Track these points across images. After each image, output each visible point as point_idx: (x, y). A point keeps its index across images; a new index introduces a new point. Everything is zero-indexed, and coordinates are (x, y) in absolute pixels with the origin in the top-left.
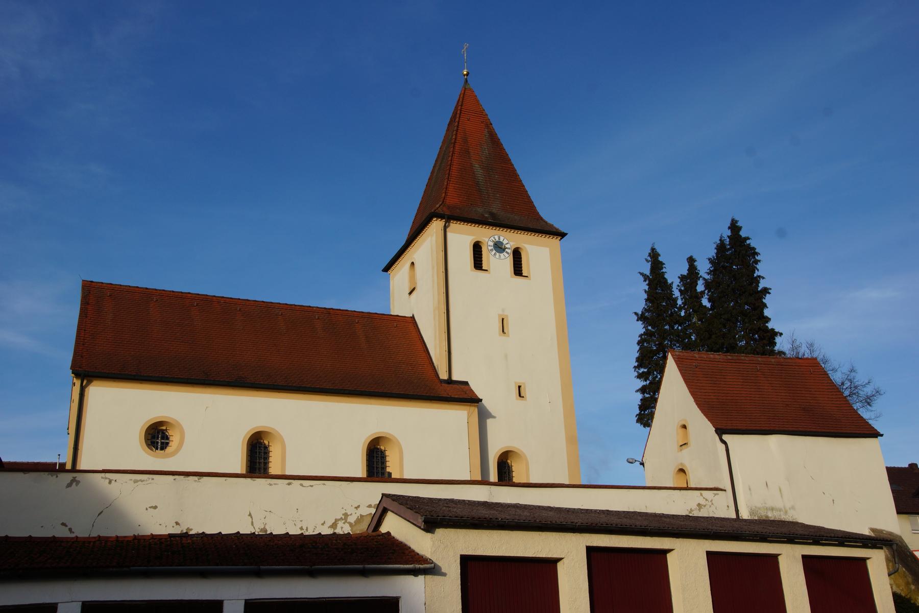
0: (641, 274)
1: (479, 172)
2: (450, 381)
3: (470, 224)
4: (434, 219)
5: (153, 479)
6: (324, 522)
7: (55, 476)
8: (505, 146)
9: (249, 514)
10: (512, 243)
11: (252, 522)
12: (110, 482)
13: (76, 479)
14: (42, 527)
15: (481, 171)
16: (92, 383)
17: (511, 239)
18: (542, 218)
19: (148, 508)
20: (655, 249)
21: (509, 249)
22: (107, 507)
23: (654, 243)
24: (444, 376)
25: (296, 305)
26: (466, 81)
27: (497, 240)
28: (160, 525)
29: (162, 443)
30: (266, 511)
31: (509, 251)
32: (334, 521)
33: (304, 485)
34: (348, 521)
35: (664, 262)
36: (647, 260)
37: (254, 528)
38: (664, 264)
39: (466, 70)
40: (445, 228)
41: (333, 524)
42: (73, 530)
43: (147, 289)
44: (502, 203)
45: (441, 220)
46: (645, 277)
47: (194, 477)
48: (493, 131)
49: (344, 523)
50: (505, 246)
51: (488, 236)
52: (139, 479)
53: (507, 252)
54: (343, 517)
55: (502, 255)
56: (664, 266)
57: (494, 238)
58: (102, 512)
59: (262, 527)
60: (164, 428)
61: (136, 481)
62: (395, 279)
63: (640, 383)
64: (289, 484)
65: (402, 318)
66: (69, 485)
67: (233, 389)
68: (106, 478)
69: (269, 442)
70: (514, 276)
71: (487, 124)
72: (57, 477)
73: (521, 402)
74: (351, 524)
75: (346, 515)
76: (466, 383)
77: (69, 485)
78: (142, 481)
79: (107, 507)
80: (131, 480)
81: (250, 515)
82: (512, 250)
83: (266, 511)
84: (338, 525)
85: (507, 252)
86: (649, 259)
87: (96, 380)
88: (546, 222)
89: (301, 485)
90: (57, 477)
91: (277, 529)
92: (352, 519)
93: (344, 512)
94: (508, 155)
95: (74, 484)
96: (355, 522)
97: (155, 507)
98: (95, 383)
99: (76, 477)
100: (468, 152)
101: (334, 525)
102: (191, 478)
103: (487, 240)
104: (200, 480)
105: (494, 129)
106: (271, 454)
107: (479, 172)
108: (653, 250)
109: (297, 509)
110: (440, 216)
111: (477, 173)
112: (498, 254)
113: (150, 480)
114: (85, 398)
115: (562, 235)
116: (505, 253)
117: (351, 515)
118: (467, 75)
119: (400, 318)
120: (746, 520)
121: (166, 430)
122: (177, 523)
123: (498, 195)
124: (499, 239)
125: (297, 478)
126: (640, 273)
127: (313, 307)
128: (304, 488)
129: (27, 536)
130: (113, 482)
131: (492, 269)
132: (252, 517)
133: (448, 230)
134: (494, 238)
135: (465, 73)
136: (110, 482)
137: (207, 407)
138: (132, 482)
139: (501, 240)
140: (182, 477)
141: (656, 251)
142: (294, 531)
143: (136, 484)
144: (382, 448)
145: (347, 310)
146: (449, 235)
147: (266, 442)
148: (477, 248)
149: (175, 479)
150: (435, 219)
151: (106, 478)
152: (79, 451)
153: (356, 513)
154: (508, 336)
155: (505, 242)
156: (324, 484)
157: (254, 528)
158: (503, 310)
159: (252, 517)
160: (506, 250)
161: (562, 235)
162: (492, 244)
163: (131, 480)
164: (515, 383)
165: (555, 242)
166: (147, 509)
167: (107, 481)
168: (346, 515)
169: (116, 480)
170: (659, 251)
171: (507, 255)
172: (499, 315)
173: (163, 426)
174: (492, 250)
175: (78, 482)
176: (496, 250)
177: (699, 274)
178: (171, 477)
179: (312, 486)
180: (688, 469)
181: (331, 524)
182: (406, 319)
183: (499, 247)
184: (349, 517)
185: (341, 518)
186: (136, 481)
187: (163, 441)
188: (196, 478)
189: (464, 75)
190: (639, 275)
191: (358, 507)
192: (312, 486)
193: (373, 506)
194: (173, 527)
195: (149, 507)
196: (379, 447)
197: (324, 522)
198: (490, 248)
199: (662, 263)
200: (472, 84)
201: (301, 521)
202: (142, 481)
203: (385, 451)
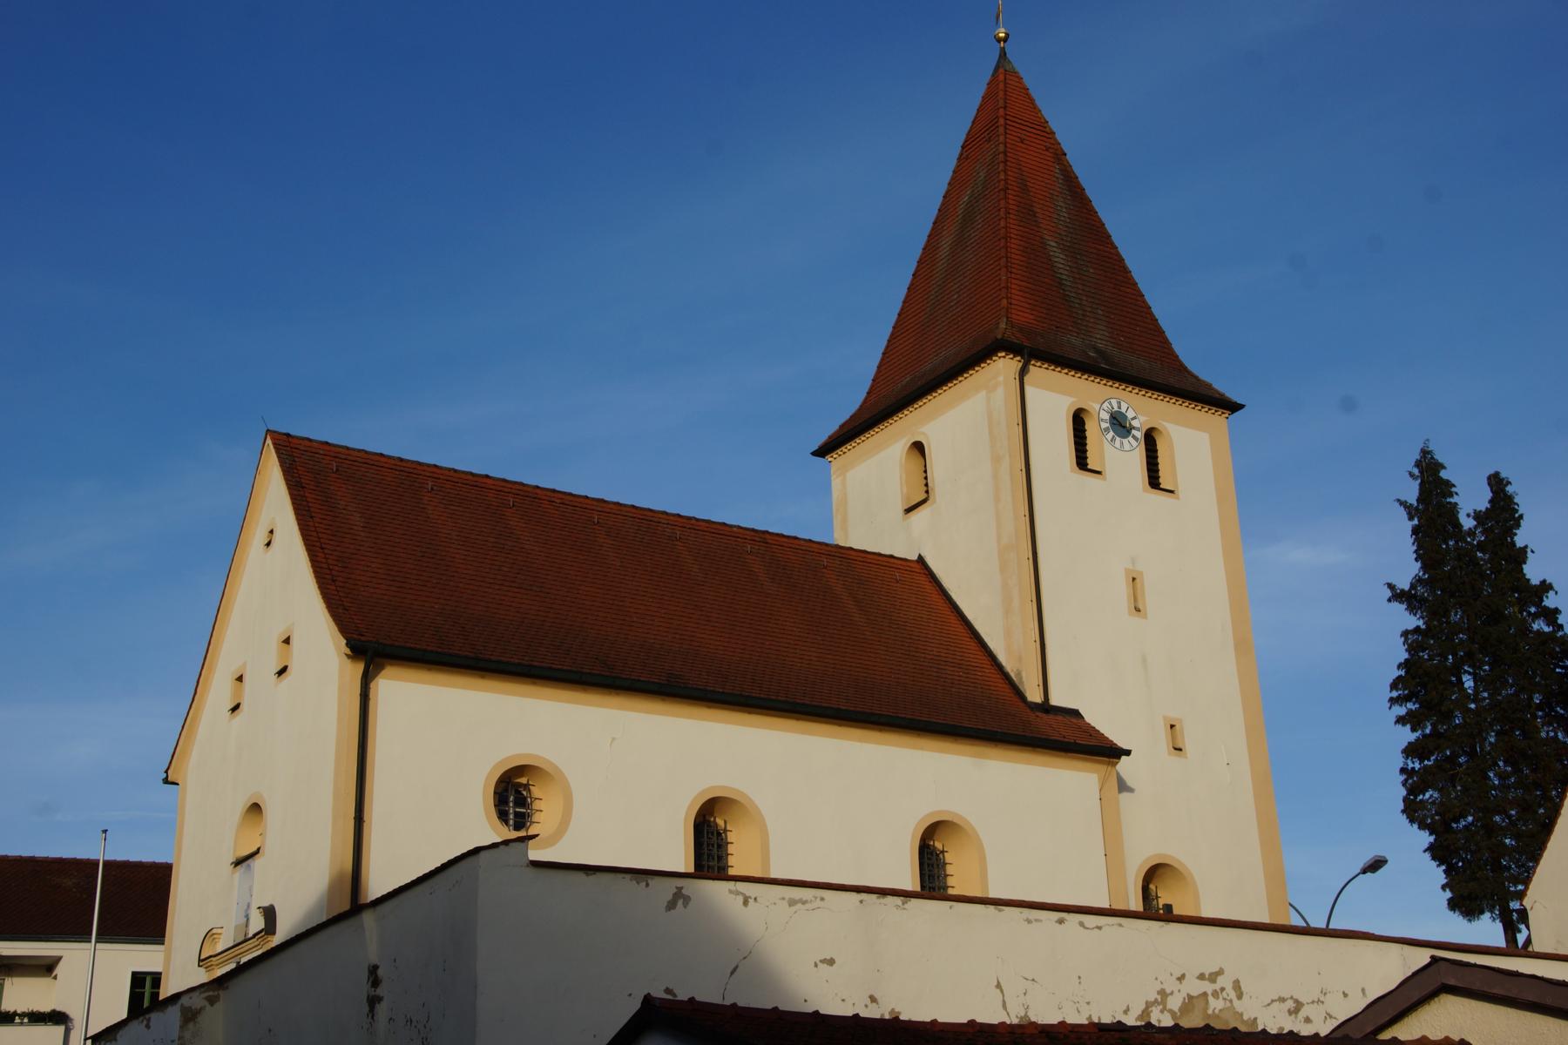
0: (1403, 503)
1: (1059, 258)
2: (1046, 708)
3: (1066, 371)
4: (1000, 355)
5: (822, 899)
6: (1128, 1006)
7: (644, 883)
8: (1096, 204)
9: (996, 984)
10: (1142, 418)
11: (1004, 1001)
12: (746, 903)
13: (684, 891)
14: (630, 995)
15: (1061, 256)
16: (383, 672)
17: (1142, 408)
18: (1185, 369)
19: (818, 962)
20: (1429, 452)
21: (1138, 429)
22: (745, 958)
23: (1428, 440)
24: (1035, 696)
25: (697, 520)
26: (1003, 54)
27: (1116, 409)
28: (843, 1000)
29: (517, 814)
30: (1027, 979)
31: (1139, 434)
32: (1143, 1007)
33: (1087, 925)
34: (1168, 1007)
35: (1453, 482)
36: (1411, 475)
37: (1008, 1014)
38: (1454, 486)
39: (1003, 30)
40: (1023, 372)
41: (1143, 1012)
42: (1125, 1008)
43: (401, 460)
44: (1110, 330)
45: (1014, 356)
46: (1411, 512)
47: (895, 898)
48: (1069, 169)
49: (1162, 1012)
50: (1130, 424)
51: (1101, 398)
52: (797, 898)
53: (1134, 437)
54: (1159, 998)
55: (1125, 441)
56: (1453, 489)
57: (1119, 403)
58: (737, 967)
59: (1023, 1014)
60: (523, 780)
61: (792, 903)
62: (849, 475)
63: (1407, 735)
64: (1061, 921)
65: (900, 562)
66: (671, 905)
67: (663, 700)
68: (738, 893)
69: (725, 822)
70: (1148, 487)
71: (1057, 154)
72: (647, 885)
73: (1175, 760)
74: (1172, 1012)
75: (1162, 993)
76: (1075, 713)
77: (671, 905)
78: (804, 903)
79: (745, 958)
80: (783, 899)
81: (999, 986)
82: (1144, 433)
83: (1027, 979)
84: (1152, 1014)
85: (1134, 437)
86: (1416, 471)
87: (391, 665)
88: (1196, 378)
89: (1082, 924)
90: (647, 885)
91: (1047, 1014)
92: (1175, 1003)
93: (1159, 988)
94: (1104, 225)
95: (680, 903)
96: (1180, 1009)
97: (831, 962)
98: (389, 671)
99: (682, 888)
100: (1033, 211)
101: (1146, 1012)
102: (890, 899)
103: (1097, 407)
104: (906, 906)
105: (1071, 166)
106: (731, 849)
107: (1059, 258)
108: (1425, 453)
109: (1079, 978)
110: (1013, 349)
111: (1056, 260)
112: (1118, 439)
113: (818, 899)
114: (371, 703)
115: (1232, 407)
116: (1130, 438)
117: (1172, 993)
118: (1005, 40)
119: (896, 561)
120: (889, 1020)
121: (526, 786)
122: (873, 999)
123: (1100, 312)
124: (1120, 408)
125: (1292, 930)
126: (1398, 500)
127: (731, 526)
128: (1086, 931)
129: (928, 1019)
130: (751, 901)
131: (1108, 471)
132: (1002, 991)
133: (1025, 378)
134: (1119, 403)
135: (1002, 35)
136: (746, 903)
137: (614, 739)
138: (785, 903)
139: (1123, 410)
140: (874, 896)
141: (1432, 458)
142: (1076, 1018)
143: (794, 908)
144: (938, 845)
145: (796, 538)
146: (1028, 389)
147: (720, 822)
148: (1079, 421)
149: (861, 902)
150: (1003, 354)
151: (738, 893)
152: (365, 824)
153: (1179, 991)
154: (1145, 617)
155: (1130, 414)
156: (1120, 925)
157: (1008, 1014)
158: (1133, 562)
159: (1002, 991)
160: (1133, 432)
161: (1232, 407)
162: (1105, 416)
163: (783, 899)
164: (1165, 718)
165: (1217, 420)
166: (816, 965)
167: (740, 899)
168: (1162, 993)
169: (755, 899)
170: (1440, 457)
171: (1134, 443)
172: (1127, 571)
173: (522, 776)
174: (1107, 430)
175: (687, 900)
176: (1114, 431)
177: (1517, 511)
178: (854, 897)
179: (1099, 928)
180: (1121, 928)
181: (1140, 1013)
182: (909, 564)
183: (1119, 424)
184: (1168, 999)
185: (1156, 999)
186: (792, 903)
187: (518, 810)
188: (898, 900)
189: (999, 40)
190: (1397, 504)
191: (1181, 978)
192: (1099, 928)
193: (1207, 976)
194: (866, 1006)
195: (821, 961)
196: (932, 843)
197: (1128, 1006)
198: (1104, 425)
199: (1448, 484)
200: (1020, 62)
201: (1088, 1003)
202: (804, 903)
203: (943, 852)
